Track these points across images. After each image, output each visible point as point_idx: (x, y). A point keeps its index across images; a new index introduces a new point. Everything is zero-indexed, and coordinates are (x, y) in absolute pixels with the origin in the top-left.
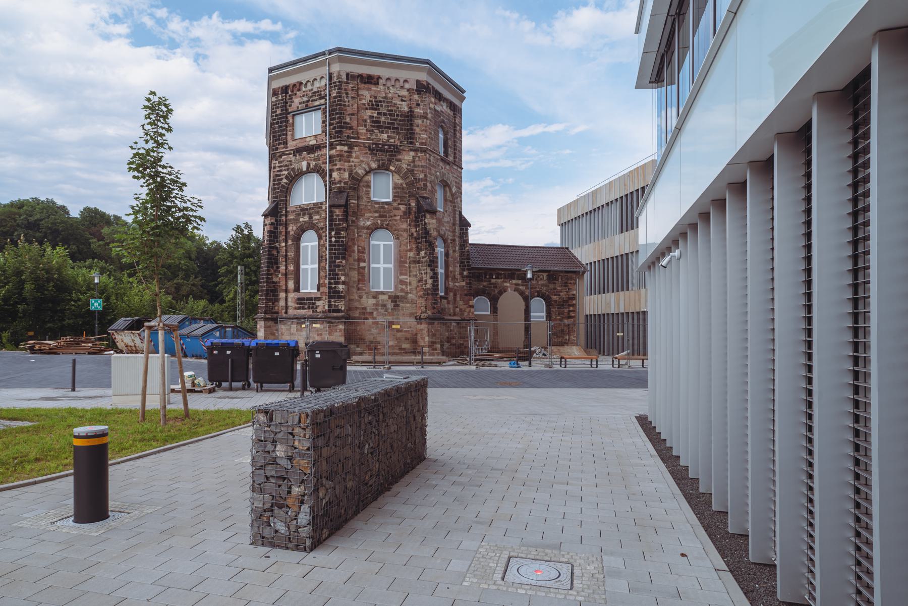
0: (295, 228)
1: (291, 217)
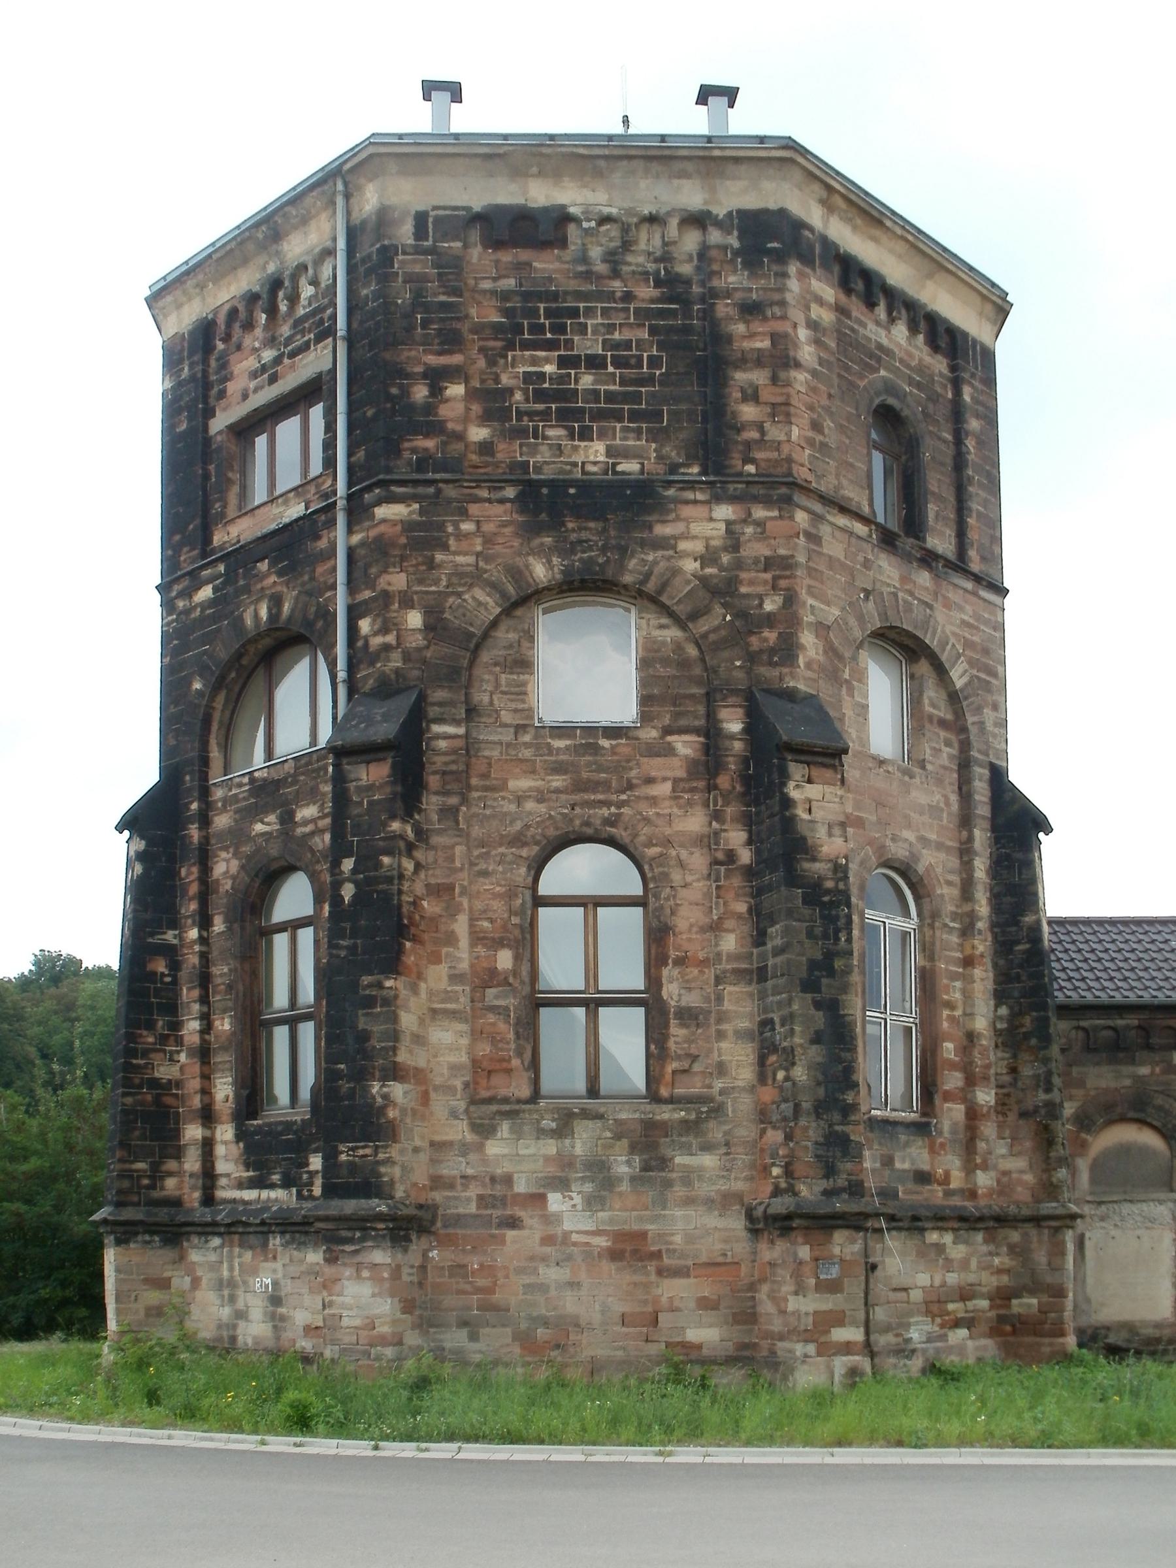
0: (235, 865)
1: (222, 821)
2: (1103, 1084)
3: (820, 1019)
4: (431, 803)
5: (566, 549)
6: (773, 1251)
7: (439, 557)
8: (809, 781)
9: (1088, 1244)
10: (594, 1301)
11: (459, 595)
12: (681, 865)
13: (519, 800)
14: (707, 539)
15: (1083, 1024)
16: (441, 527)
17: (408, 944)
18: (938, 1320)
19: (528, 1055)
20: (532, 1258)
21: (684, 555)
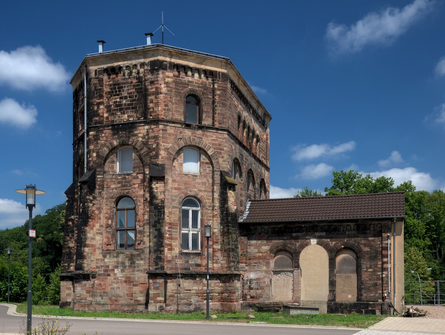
3: (156, 233)
4: (97, 191)
5: (119, 138)
7: (99, 142)
9: (272, 281)
10: (122, 290)
11: (102, 149)
12: (140, 201)
13: (113, 189)
16: (99, 135)
18: (201, 297)
21: (139, 137)
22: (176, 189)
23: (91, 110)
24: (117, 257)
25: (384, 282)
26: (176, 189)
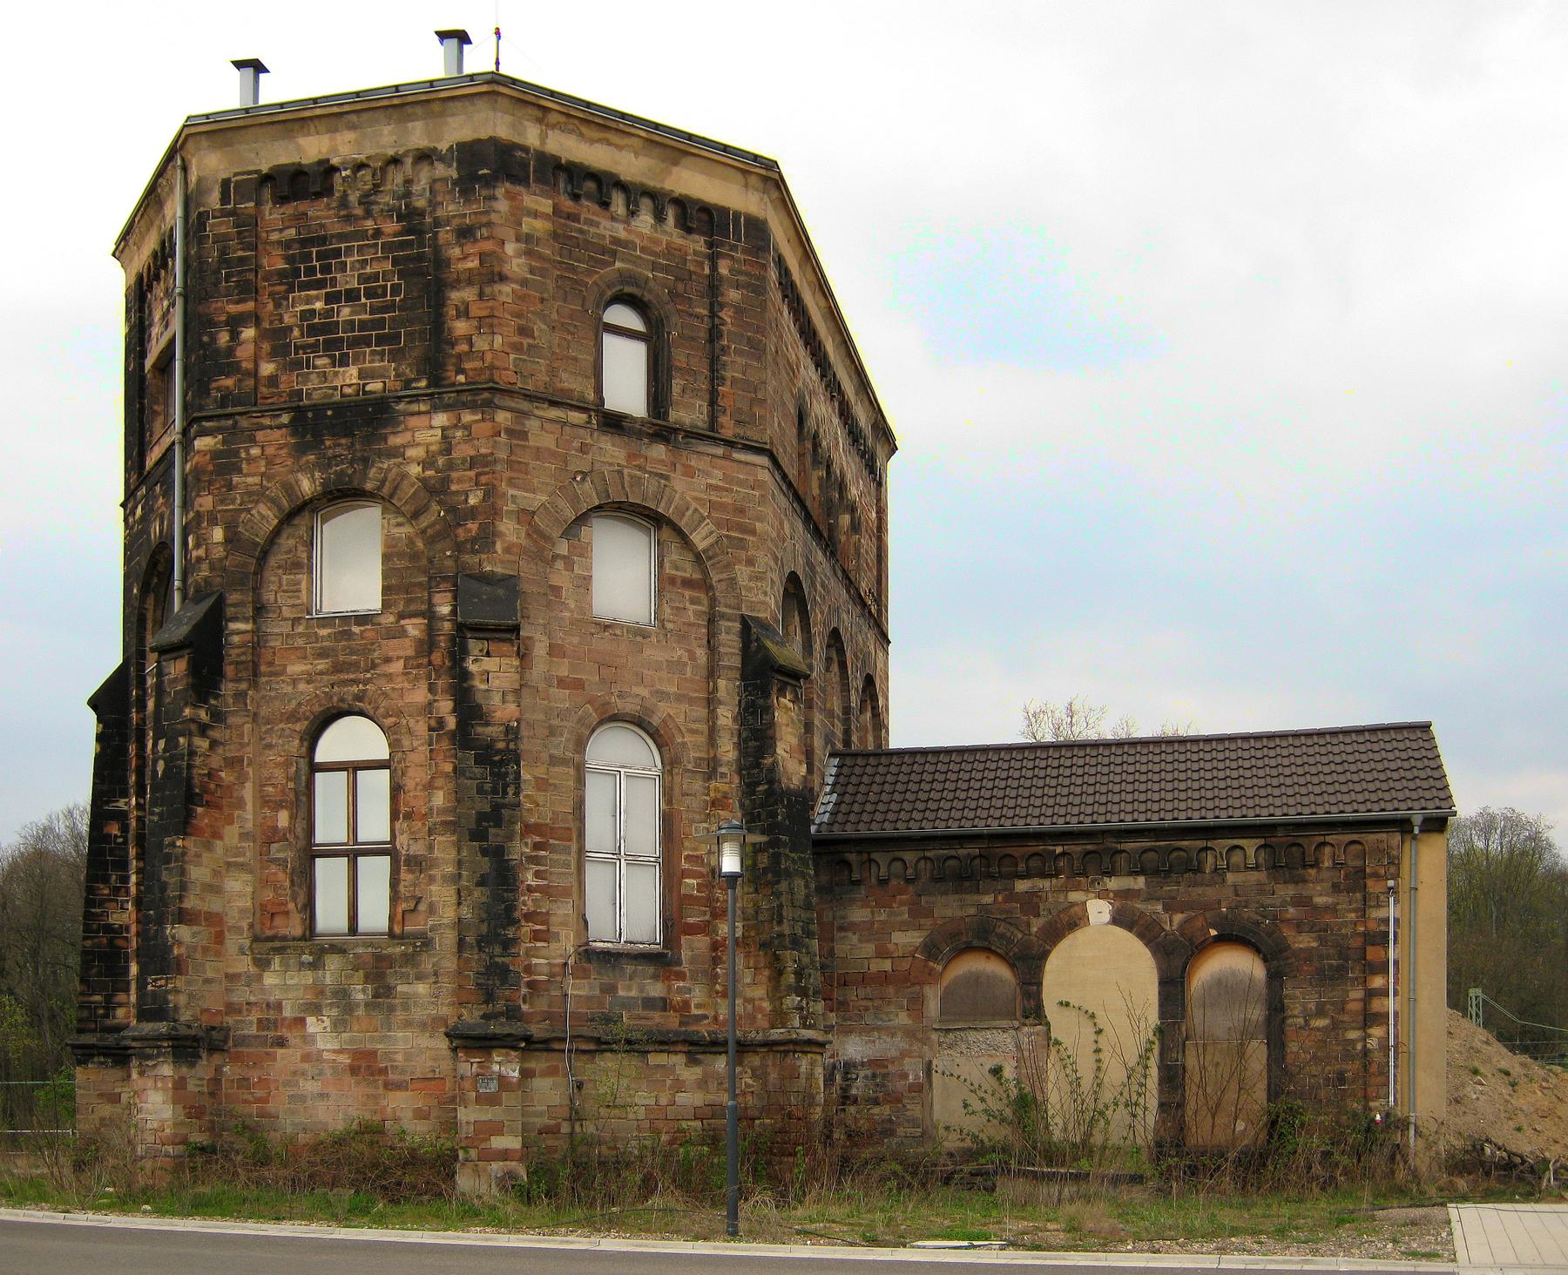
2: (949, 913)
3: (485, 864)
4: (228, 688)
5: (325, 464)
6: (468, 1067)
7: (236, 479)
8: (488, 654)
11: (248, 511)
12: (410, 731)
14: (428, 445)
15: (928, 854)
16: (237, 452)
17: (199, 810)
19: (301, 899)
20: (295, 1073)
22: (562, 683)
23: (202, 345)
24: (315, 965)
25: (1374, 1068)
26: (562, 683)
